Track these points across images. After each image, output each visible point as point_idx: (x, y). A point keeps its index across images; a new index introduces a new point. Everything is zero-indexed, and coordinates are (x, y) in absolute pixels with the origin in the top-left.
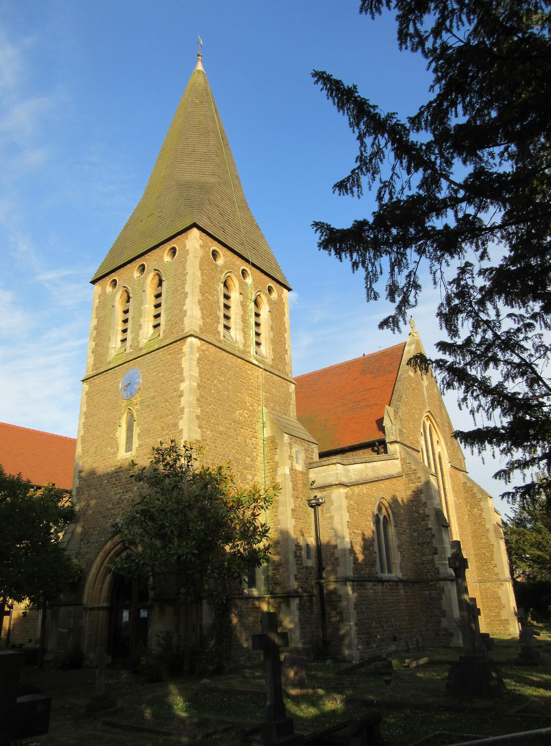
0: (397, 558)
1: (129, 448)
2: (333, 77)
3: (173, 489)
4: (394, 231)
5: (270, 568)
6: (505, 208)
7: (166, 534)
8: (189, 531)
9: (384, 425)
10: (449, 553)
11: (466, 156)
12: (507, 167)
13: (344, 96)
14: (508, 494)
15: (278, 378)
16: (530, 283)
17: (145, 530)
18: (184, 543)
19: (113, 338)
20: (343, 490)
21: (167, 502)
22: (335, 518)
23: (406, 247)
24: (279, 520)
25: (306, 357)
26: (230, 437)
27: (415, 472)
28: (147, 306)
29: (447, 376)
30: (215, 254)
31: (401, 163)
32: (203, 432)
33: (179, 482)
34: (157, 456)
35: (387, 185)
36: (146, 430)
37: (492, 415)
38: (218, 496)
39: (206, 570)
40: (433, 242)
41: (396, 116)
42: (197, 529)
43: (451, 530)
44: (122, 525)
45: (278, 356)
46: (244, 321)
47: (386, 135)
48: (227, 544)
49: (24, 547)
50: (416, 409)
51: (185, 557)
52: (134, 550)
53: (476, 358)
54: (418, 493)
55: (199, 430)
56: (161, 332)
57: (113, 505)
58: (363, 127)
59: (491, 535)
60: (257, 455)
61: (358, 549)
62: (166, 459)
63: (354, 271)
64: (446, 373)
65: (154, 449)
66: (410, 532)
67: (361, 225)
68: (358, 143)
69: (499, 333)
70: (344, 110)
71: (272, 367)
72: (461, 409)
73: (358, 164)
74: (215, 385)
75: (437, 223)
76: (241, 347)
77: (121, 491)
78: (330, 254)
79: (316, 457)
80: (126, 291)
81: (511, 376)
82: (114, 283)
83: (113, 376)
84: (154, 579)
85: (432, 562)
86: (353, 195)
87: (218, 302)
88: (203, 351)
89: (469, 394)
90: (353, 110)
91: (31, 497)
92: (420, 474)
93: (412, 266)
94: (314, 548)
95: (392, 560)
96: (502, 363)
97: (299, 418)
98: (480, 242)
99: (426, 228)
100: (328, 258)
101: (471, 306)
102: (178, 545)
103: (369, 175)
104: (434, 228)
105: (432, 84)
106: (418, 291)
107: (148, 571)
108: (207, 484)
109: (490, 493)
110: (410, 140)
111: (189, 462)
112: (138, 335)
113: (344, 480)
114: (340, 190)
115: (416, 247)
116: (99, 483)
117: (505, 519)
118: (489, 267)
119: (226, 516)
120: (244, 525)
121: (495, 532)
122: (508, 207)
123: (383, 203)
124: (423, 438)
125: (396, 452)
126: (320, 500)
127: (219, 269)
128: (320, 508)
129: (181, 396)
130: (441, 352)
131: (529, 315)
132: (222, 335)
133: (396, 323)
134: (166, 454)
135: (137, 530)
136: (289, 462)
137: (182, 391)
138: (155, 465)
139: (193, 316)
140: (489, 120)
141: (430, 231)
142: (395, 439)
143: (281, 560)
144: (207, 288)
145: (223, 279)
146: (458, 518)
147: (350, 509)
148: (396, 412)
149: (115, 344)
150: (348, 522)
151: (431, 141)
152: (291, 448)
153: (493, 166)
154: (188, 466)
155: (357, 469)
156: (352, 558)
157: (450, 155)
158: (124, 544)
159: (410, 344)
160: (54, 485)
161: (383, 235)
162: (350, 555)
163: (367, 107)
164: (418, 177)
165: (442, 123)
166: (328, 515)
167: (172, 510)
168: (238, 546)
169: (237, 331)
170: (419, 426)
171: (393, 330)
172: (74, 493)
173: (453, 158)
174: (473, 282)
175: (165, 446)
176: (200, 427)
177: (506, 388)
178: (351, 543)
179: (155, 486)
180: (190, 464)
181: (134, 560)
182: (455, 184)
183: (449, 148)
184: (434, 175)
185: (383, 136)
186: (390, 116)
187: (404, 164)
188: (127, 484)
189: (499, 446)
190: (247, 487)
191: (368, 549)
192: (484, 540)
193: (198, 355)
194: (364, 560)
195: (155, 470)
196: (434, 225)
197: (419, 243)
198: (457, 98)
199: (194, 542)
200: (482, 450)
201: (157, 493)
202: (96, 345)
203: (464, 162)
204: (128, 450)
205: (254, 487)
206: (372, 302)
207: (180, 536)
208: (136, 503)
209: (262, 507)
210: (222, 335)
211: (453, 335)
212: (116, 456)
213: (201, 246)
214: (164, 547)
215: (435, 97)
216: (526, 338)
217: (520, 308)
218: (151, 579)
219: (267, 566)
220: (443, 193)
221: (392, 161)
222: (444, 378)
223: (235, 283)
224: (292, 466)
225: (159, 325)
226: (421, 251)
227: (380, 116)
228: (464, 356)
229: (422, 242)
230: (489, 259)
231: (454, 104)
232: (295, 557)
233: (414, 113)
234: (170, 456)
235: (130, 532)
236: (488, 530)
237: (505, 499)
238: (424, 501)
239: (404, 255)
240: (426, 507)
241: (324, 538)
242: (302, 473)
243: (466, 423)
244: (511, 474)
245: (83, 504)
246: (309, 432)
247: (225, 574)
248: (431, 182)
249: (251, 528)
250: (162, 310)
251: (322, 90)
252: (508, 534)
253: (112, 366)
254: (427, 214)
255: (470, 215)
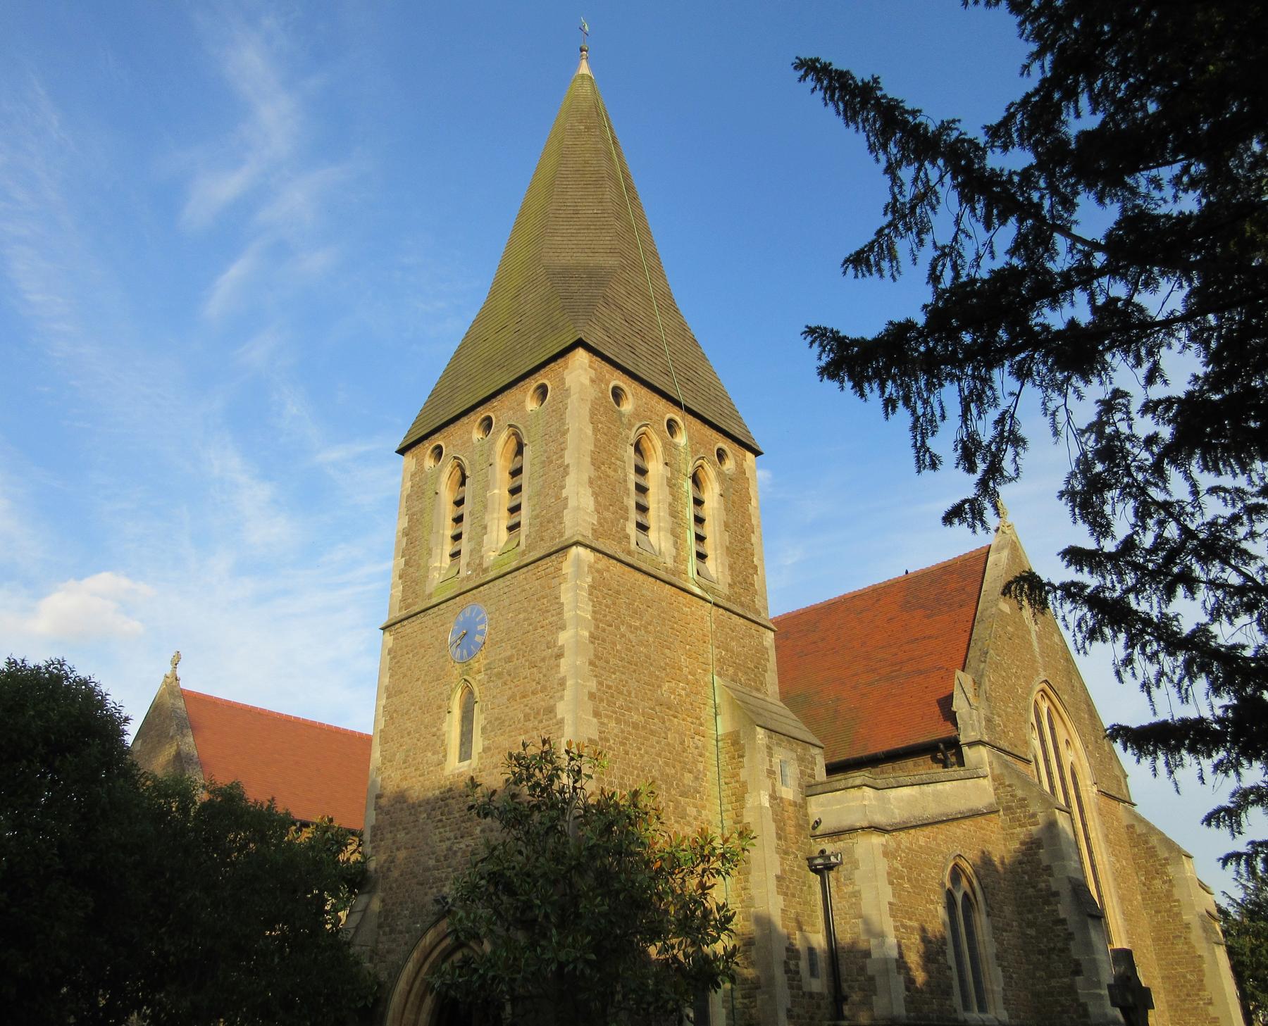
0: (995, 981)
1: (465, 754)
2: (834, 67)
3: (547, 833)
4: (967, 338)
5: (738, 994)
6: (1190, 281)
7: (536, 920)
8: (578, 916)
9: (954, 709)
10: (1108, 973)
11: (1103, 190)
12: (1190, 203)
13: (855, 97)
14: (1237, 856)
15: (742, 620)
16: (1253, 425)
17: (497, 912)
18: (570, 939)
19: (436, 551)
20: (877, 840)
21: (537, 859)
22: (863, 896)
23: (990, 367)
24: (751, 898)
25: (793, 581)
26: (652, 733)
27: (1023, 802)
28: (496, 491)
29: (1089, 615)
30: (617, 394)
31: (973, 210)
32: (602, 723)
33: (559, 819)
34: (517, 770)
35: (948, 253)
36: (496, 719)
37: (1190, 692)
38: (632, 847)
39: (613, 994)
40: (1046, 355)
41: (957, 125)
42: (593, 913)
43: (1107, 925)
44: (454, 900)
45: (740, 579)
46: (674, 514)
47: (940, 162)
48: (652, 942)
49: (276, 937)
50: (1018, 678)
51: (571, 967)
52: (476, 948)
53: (1147, 577)
54: (1032, 846)
55: (595, 720)
56: (523, 539)
57: (437, 861)
58: (895, 151)
59: (1196, 934)
60: (705, 768)
61: (913, 959)
62: (534, 775)
63: (887, 415)
64: (1085, 609)
65: (511, 756)
66: (1020, 926)
67: (900, 333)
68: (887, 180)
69: (1193, 527)
70: (856, 123)
71: (729, 599)
72: (1121, 681)
73: (889, 217)
74: (623, 636)
75: (1054, 318)
76: (670, 563)
77: (452, 835)
78: (842, 388)
79: (820, 773)
80: (459, 465)
81: (1226, 612)
82: (438, 452)
83: (437, 620)
84: (513, 1009)
85: (1071, 990)
86: (882, 276)
87: (625, 481)
88: (598, 571)
89: (1137, 649)
90: (875, 122)
91: (290, 842)
92: (1035, 807)
93: (1004, 403)
94: (823, 955)
95: (987, 985)
96: (1203, 586)
97: (785, 697)
98: (1143, 352)
99: (1031, 328)
100: (840, 394)
101: (1130, 475)
102: (558, 943)
103: (912, 236)
104: (1046, 328)
105: (1026, 62)
106: (1020, 450)
107: (502, 992)
108: (611, 824)
109: (1185, 847)
110: (988, 167)
111: (576, 781)
112: (480, 544)
113: (880, 819)
114: (855, 268)
115: (1011, 366)
116: (412, 818)
117: (1224, 903)
118: (1163, 396)
119: (649, 887)
120: (685, 906)
121: (1205, 930)
122: (1196, 283)
123: (942, 286)
124: (1035, 735)
125: (981, 761)
126: (833, 859)
127: (625, 420)
128: (832, 874)
129: (560, 656)
130: (1073, 568)
131: (1255, 489)
132: (633, 541)
133: (978, 514)
134: (533, 767)
135: (484, 912)
136: (768, 782)
137: (562, 647)
138: (513, 787)
139: (580, 506)
140: (1143, 119)
141: (1039, 334)
142: (979, 738)
143: (758, 977)
144: (604, 455)
145: (633, 439)
146: (1122, 899)
147: (894, 878)
148: (977, 684)
149: (440, 561)
150: (890, 903)
151: (1031, 167)
152: (771, 755)
153: (1160, 202)
154: (575, 788)
155: (903, 797)
156: (901, 978)
157: (1069, 189)
158: (457, 938)
159: (999, 550)
160: (331, 820)
161: (945, 346)
162: (899, 973)
163: (902, 114)
164: (1007, 233)
165: (1050, 129)
166: (850, 889)
167: (545, 873)
168: (673, 947)
169: (662, 533)
170: (1027, 710)
171: (973, 527)
172: (367, 837)
173: (1076, 193)
174: (1130, 427)
175: (533, 750)
176: (596, 714)
177: (1215, 637)
178: (899, 946)
179: (513, 826)
180: (578, 785)
181: (476, 970)
182: (1084, 242)
183: (1066, 176)
184: (1040, 228)
185: (933, 163)
186: (946, 127)
187: (978, 212)
188: (463, 821)
189: (1210, 756)
190: (688, 830)
191: (935, 961)
192: (1180, 947)
193: (589, 580)
194: (927, 983)
195: (514, 796)
196: (1046, 322)
197: (1017, 358)
198: (1077, 83)
199: (589, 938)
200: (1176, 766)
201: (518, 839)
202: (406, 563)
203: (1100, 200)
204: (462, 756)
205: (703, 833)
206: (927, 473)
207: (561, 926)
208: (479, 858)
209: (718, 872)
210: (633, 541)
211: (1101, 533)
212: (443, 769)
213: (593, 381)
214: (533, 945)
215: (1037, 84)
216: (1252, 535)
217: (1235, 475)
218: (508, 1008)
219: (732, 989)
220: (1062, 260)
221: (955, 208)
222: (1082, 618)
223: (655, 446)
224: (774, 791)
225: (518, 525)
226: (1022, 374)
227: (926, 128)
228: (1120, 575)
229: (1023, 355)
230: (1165, 382)
231: (1071, 95)
232: (786, 972)
233: (996, 118)
234: (541, 770)
235: (468, 915)
236: (1187, 926)
237: (1231, 867)
238: (1045, 862)
239: (987, 381)
240: (1051, 875)
241: (846, 933)
242: (795, 804)
243: (1125, 704)
244: (1243, 814)
245: (383, 857)
246: (804, 723)
247: (649, 1004)
248: (1035, 242)
249: (698, 913)
250: (524, 498)
251: (813, 91)
252: (1231, 935)
253: (435, 601)
254: (1030, 303)
255: (1119, 299)
